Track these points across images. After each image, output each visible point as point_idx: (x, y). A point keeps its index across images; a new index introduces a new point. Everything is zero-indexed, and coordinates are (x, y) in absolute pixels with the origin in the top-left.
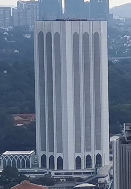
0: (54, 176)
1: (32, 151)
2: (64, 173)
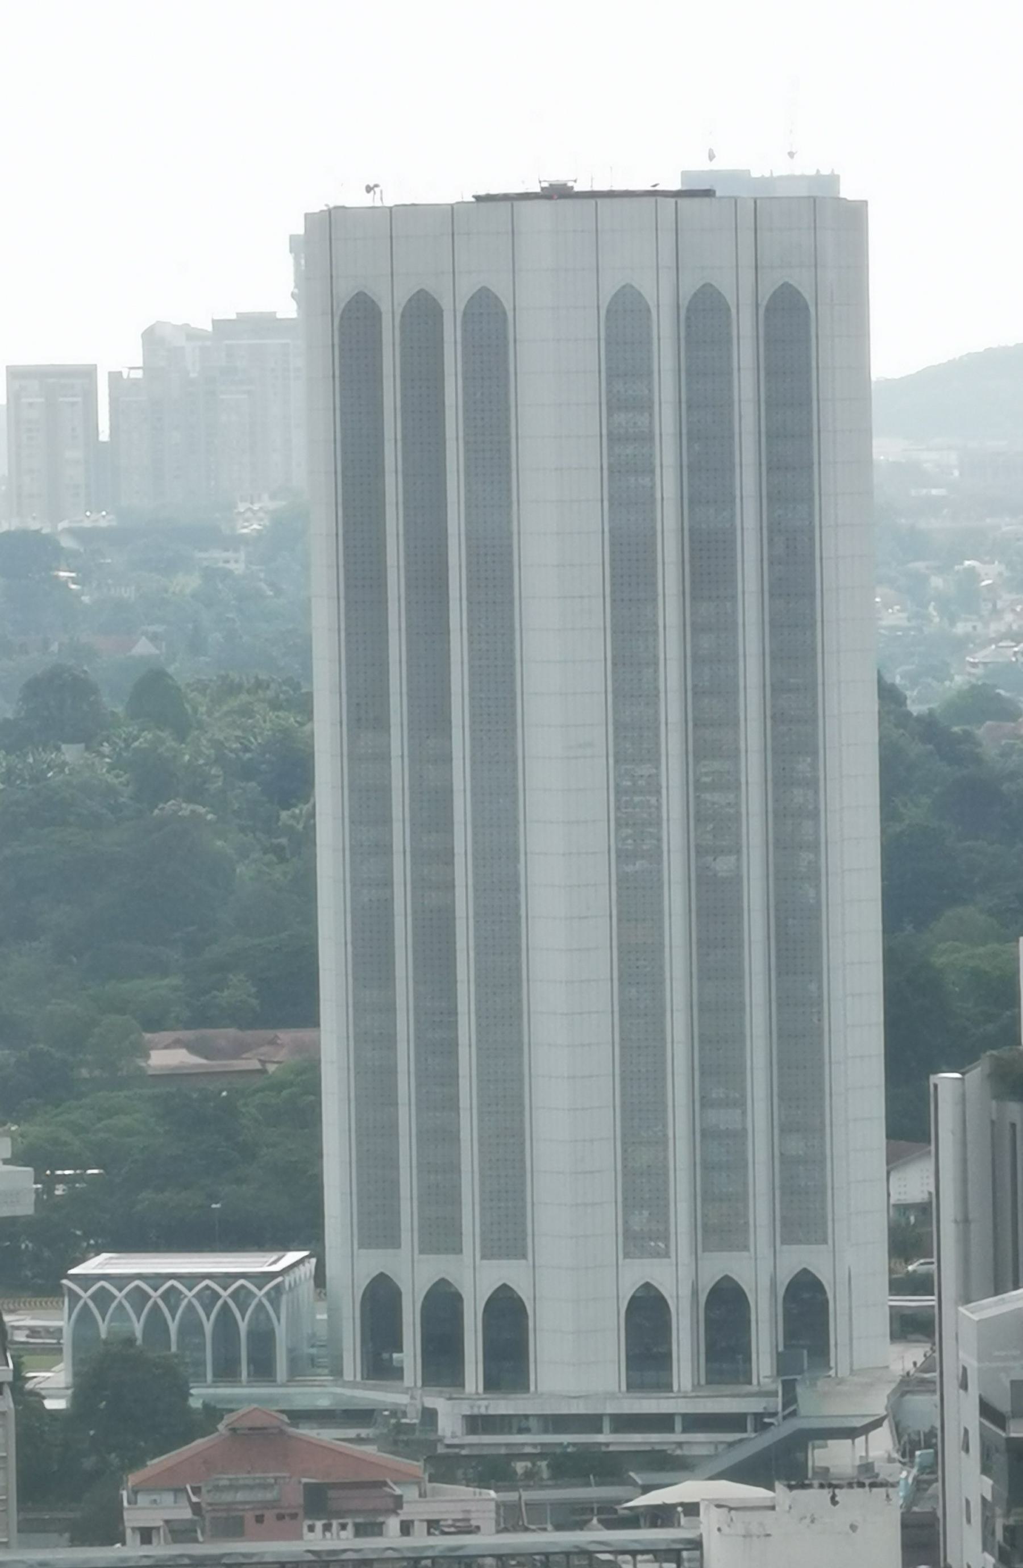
0: (461, 1446)
1: (292, 1257)
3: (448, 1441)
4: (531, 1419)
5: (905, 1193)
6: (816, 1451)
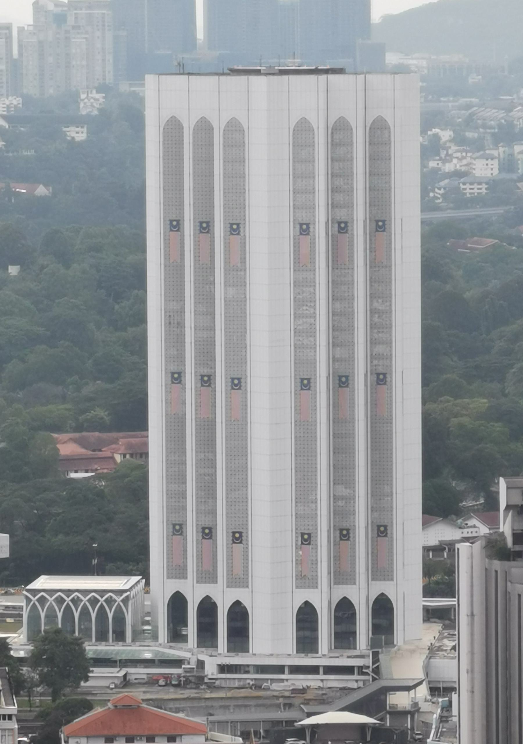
0: (216, 679)
2: (290, 667)
3: (210, 677)
4: (250, 666)
5: (427, 541)
6: (391, 696)
